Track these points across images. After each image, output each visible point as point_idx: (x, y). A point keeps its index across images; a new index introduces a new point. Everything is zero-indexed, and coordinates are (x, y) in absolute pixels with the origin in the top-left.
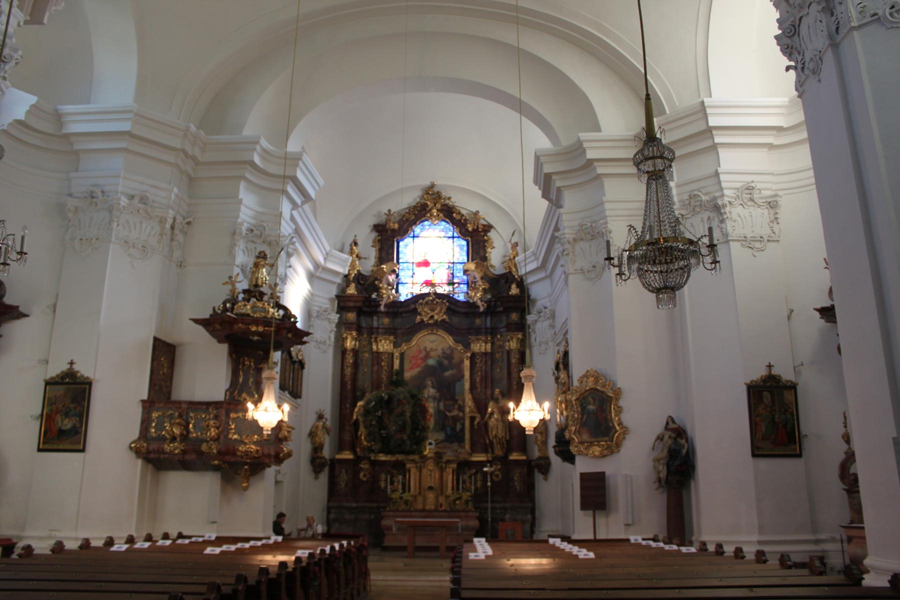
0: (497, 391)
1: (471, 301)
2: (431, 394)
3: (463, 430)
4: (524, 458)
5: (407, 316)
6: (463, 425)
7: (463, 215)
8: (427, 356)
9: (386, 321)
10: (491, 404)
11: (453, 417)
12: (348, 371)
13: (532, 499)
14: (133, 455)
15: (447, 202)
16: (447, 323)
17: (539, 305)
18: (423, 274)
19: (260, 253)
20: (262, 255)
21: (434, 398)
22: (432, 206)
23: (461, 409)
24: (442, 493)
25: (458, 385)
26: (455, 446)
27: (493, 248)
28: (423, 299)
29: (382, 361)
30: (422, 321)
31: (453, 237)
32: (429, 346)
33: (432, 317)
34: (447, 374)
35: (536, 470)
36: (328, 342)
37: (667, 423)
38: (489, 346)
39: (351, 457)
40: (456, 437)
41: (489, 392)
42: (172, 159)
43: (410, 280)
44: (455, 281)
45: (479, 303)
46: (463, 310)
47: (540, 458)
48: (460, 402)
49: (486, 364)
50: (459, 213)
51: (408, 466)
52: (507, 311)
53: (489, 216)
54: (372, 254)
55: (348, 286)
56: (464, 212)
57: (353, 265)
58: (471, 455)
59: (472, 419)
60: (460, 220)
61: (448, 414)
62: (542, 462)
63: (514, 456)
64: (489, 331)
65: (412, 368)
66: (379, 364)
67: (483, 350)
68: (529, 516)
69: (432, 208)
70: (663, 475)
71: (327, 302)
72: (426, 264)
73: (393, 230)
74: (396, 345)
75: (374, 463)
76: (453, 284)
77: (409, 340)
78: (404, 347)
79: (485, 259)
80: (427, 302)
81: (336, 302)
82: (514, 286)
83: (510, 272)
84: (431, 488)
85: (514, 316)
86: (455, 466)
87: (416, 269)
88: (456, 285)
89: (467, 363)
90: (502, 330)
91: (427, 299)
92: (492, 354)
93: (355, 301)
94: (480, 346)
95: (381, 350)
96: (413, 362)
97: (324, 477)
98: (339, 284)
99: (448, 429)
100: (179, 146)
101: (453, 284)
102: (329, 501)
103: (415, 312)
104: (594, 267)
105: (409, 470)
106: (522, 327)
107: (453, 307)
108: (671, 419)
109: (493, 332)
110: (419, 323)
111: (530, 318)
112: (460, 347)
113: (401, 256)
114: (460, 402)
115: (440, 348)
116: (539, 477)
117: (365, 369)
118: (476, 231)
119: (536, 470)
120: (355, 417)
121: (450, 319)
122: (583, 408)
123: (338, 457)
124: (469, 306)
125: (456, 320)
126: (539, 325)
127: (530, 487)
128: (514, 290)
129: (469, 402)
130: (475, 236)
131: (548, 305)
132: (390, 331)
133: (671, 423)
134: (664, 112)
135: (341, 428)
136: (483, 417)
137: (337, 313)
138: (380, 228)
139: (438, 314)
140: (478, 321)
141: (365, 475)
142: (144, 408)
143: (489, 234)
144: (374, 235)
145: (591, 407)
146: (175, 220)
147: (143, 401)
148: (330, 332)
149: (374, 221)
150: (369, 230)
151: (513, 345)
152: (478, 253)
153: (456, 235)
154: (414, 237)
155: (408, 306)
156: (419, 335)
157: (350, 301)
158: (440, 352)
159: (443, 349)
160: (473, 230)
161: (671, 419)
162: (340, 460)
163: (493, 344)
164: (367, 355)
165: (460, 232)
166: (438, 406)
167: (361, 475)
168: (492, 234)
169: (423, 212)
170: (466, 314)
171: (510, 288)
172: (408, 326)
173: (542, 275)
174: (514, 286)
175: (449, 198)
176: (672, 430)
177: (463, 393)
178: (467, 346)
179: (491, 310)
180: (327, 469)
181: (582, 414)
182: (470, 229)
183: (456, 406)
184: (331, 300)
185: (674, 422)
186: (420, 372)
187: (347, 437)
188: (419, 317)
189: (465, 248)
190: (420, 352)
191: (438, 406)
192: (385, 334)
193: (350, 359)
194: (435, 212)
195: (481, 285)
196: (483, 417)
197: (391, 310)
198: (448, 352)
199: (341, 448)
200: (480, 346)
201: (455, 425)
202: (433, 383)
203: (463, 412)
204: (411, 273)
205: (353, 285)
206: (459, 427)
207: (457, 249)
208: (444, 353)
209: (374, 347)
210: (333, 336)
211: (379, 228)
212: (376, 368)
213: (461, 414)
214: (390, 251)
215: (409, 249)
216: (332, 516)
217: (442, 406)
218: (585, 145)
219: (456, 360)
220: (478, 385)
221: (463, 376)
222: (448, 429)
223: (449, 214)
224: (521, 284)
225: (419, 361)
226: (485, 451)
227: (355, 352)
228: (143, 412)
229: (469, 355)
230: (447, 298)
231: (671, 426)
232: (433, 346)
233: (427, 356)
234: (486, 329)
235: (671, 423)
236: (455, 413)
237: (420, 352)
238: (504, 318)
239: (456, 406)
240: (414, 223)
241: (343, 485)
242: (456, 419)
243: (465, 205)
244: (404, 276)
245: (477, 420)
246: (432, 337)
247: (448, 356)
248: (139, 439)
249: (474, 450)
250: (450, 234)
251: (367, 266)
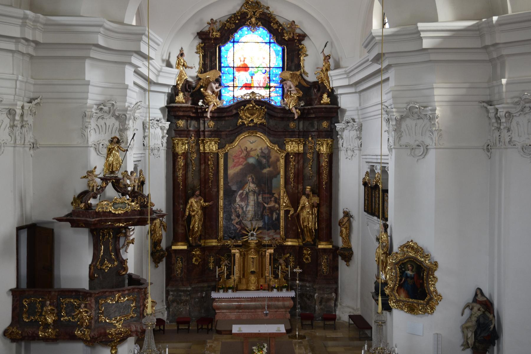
0: (308, 188)
1: (287, 108)
2: (251, 189)
3: (278, 219)
4: (331, 246)
5: (231, 119)
6: (279, 215)
7: (280, 25)
8: (248, 156)
9: (212, 124)
10: (304, 198)
11: (270, 208)
12: (180, 173)
13: (335, 280)
14: (8, 341)
15: (265, 11)
16: (265, 126)
17: (347, 116)
18: (243, 77)
19: (113, 138)
20: (115, 140)
21: (254, 192)
22: (254, 15)
23: (277, 201)
24: (262, 276)
25: (274, 181)
26: (272, 232)
27: (307, 55)
28: (245, 106)
29: (209, 160)
30: (243, 123)
31: (270, 43)
32: (250, 146)
33: (252, 120)
34: (265, 171)
35: (340, 258)
36: (161, 148)
37: (476, 295)
38: (301, 148)
39: (185, 247)
40: (274, 226)
41: (300, 187)
42: (11, 46)
43: (231, 84)
44: (272, 84)
45: (294, 110)
46: (279, 115)
47: (343, 249)
48: (276, 195)
49: (298, 163)
50: (277, 22)
51: (233, 251)
52: (321, 119)
53: (305, 26)
54: (194, 59)
55: (177, 95)
56: (281, 21)
57: (180, 76)
58: (285, 240)
59: (287, 212)
60: (277, 30)
61: (266, 205)
62: (346, 253)
63: (322, 246)
64: (302, 134)
65: (234, 166)
66: (206, 163)
67: (296, 149)
68: (334, 295)
69: (251, 17)
70: (471, 341)
71: (159, 112)
72: (245, 68)
73: (216, 39)
74: (221, 146)
75: (204, 249)
76: (270, 87)
77: (232, 141)
78: (228, 147)
79: (298, 67)
80: (248, 109)
81: (167, 110)
82: (325, 96)
83: (322, 83)
84: (253, 273)
85: (325, 124)
86: (272, 251)
87: (236, 74)
88: (272, 89)
89: (282, 161)
90: (313, 134)
91: (248, 106)
92: (304, 154)
93: (183, 111)
94: (292, 147)
95: (208, 150)
96: (235, 161)
97: (162, 265)
98: (168, 93)
99: (266, 218)
100: (18, 35)
101: (270, 87)
102: (167, 285)
103: (237, 116)
104: (418, 146)
105: (234, 255)
106: (331, 134)
107: (271, 112)
108: (479, 292)
109: (302, 136)
110: (240, 126)
111: (339, 126)
112: (276, 148)
113: (223, 60)
114: (276, 195)
115: (258, 149)
116: (342, 263)
117: (193, 168)
118: (291, 40)
119: (340, 258)
120: (187, 213)
121: (268, 122)
122: (402, 273)
123: (174, 247)
124: (283, 113)
125: (272, 122)
126: (346, 134)
127: (335, 268)
128: (325, 99)
129: (285, 201)
130: (290, 42)
131: (356, 117)
132: (215, 133)
133: (479, 295)
134: (505, 11)
135: (175, 221)
136: (296, 210)
137: (168, 121)
138: (204, 37)
139: (257, 117)
140: (292, 125)
141: (196, 260)
142: (13, 295)
143: (303, 42)
144: (198, 41)
145: (409, 273)
146: (23, 107)
147: (12, 291)
148: (163, 137)
149: (198, 28)
150: (192, 37)
151: (324, 149)
152: (292, 61)
153: (272, 41)
154: (234, 42)
155: (231, 111)
156: (242, 137)
157: (180, 111)
158: (258, 152)
159: (261, 149)
160: (289, 39)
161: (479, 292)
162: (176, 250)
163: (305, 145)
164: (195, 155)
165: (276, 40)
166: (258, 199)
168: (306, 43)
169: (243, 20)
170: (282, 118)
171: (321, 98)
172: (231, 128)
173: (352, 90)
174: (325, 96)
175: (268, 8)
176: (481, 303)
177: (279, 188)
178: (282, 147)
179: (304, 115)
180: (164, 259)
181: (401, 277)
182: (286, 38)
183: (273, 199)
184: (162, 109)
185: (482, 294)
186: (241, 169)
187: (181, 231)
188: (240, 120)
189: (281, 53)
190: (242, 151)
191: (258, 199)
192: (210, 136)
193: (181, 162)
194: (253, 20)
195: (295, 94)
196: (296, 210)
197: (216, 115)
198: (266, 152)
199: (175, 241)
200: (292, 147)
201: (272, 215)
202: (253, 179)
203: (279, 204)
204: (231, 77)
205: (181, 95)
206: (275, 216)
207: (273, 54)
208: (262, 152)
209: (201, 148)
210: (165, 140)
211: (202, 35)
212: (203, 167)
213: (277, 206)
214: (213, 59)
215: (231, 54)
216: (170, 297)
217: (260, 199)
218: (423, 35)
219: (273, 158)
220: (292, 180)
221: (279, 173)
222: (266, 218)
223: (267, 21)
224: (332, 95)
225: (241, 160)
226: (296, 236)
227: (186, 155)
228: (13, 300)
229: (284, 155)
230: (264, 104)
231: (480, 298)
232: (253, 146)
233: (248, 156)
234: (299, 132)
235: (479, 295)
236: (272, 204)
237: (242, 151)
238: (316, 123)
239: (273, 199)
240: (235, 31)
241: (179, 271)
242: (272, 210)
243: (283, 13)
244: (226, 79)
245: (292, 212)
246: (252, 139)
247: (266, 155)
248: (11, 325)
249: (287, 236)
250: (267, 40)
251: (192, 74)
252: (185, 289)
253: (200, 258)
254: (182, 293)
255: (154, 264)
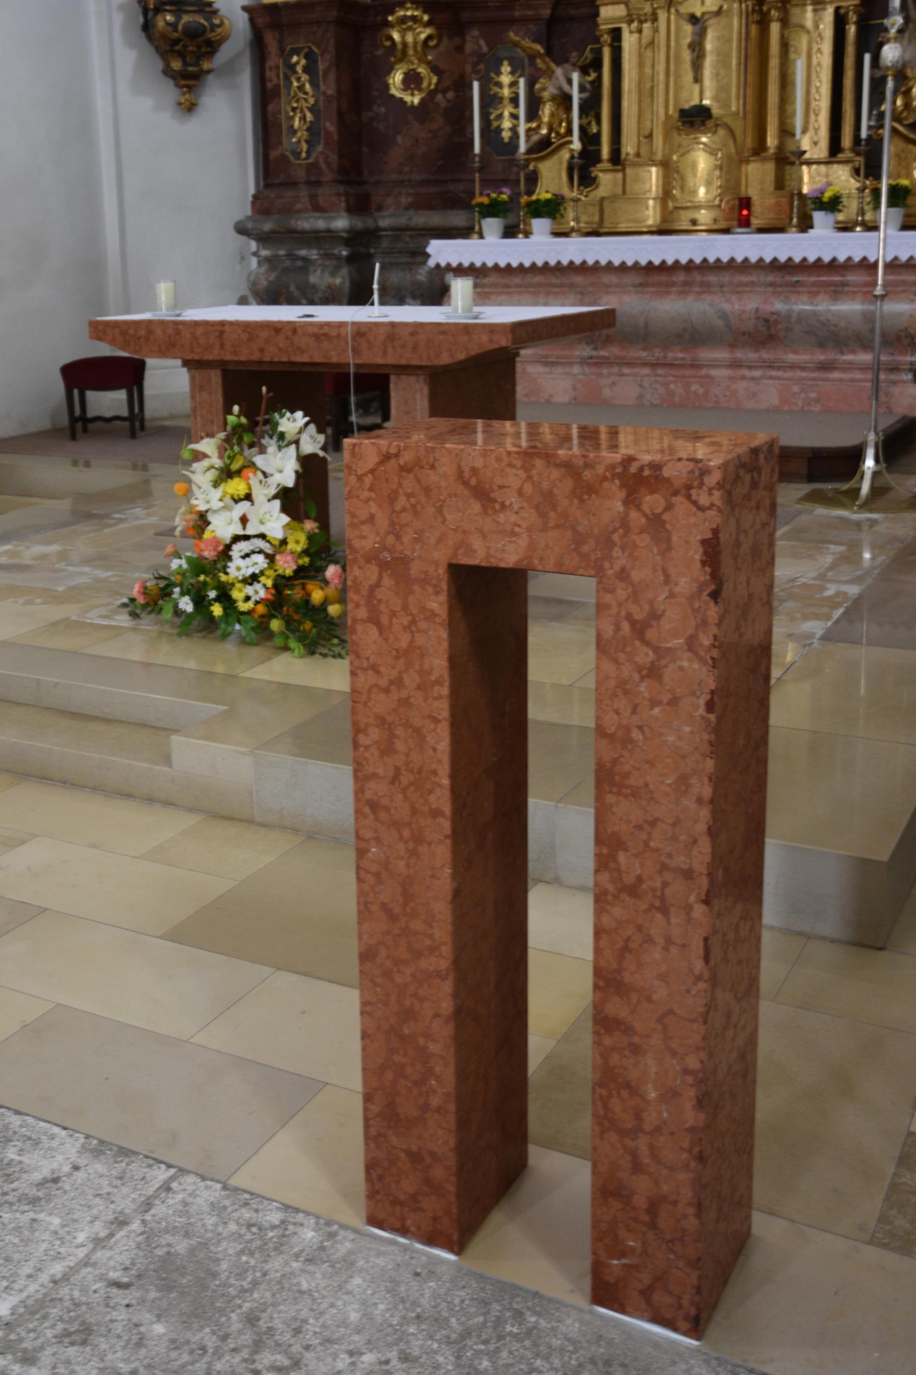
141: (412, 81)
167: (397, 78)
252: (321, 224)
253: (435, 69)
254: (313, 254)
255: (169, 92)
